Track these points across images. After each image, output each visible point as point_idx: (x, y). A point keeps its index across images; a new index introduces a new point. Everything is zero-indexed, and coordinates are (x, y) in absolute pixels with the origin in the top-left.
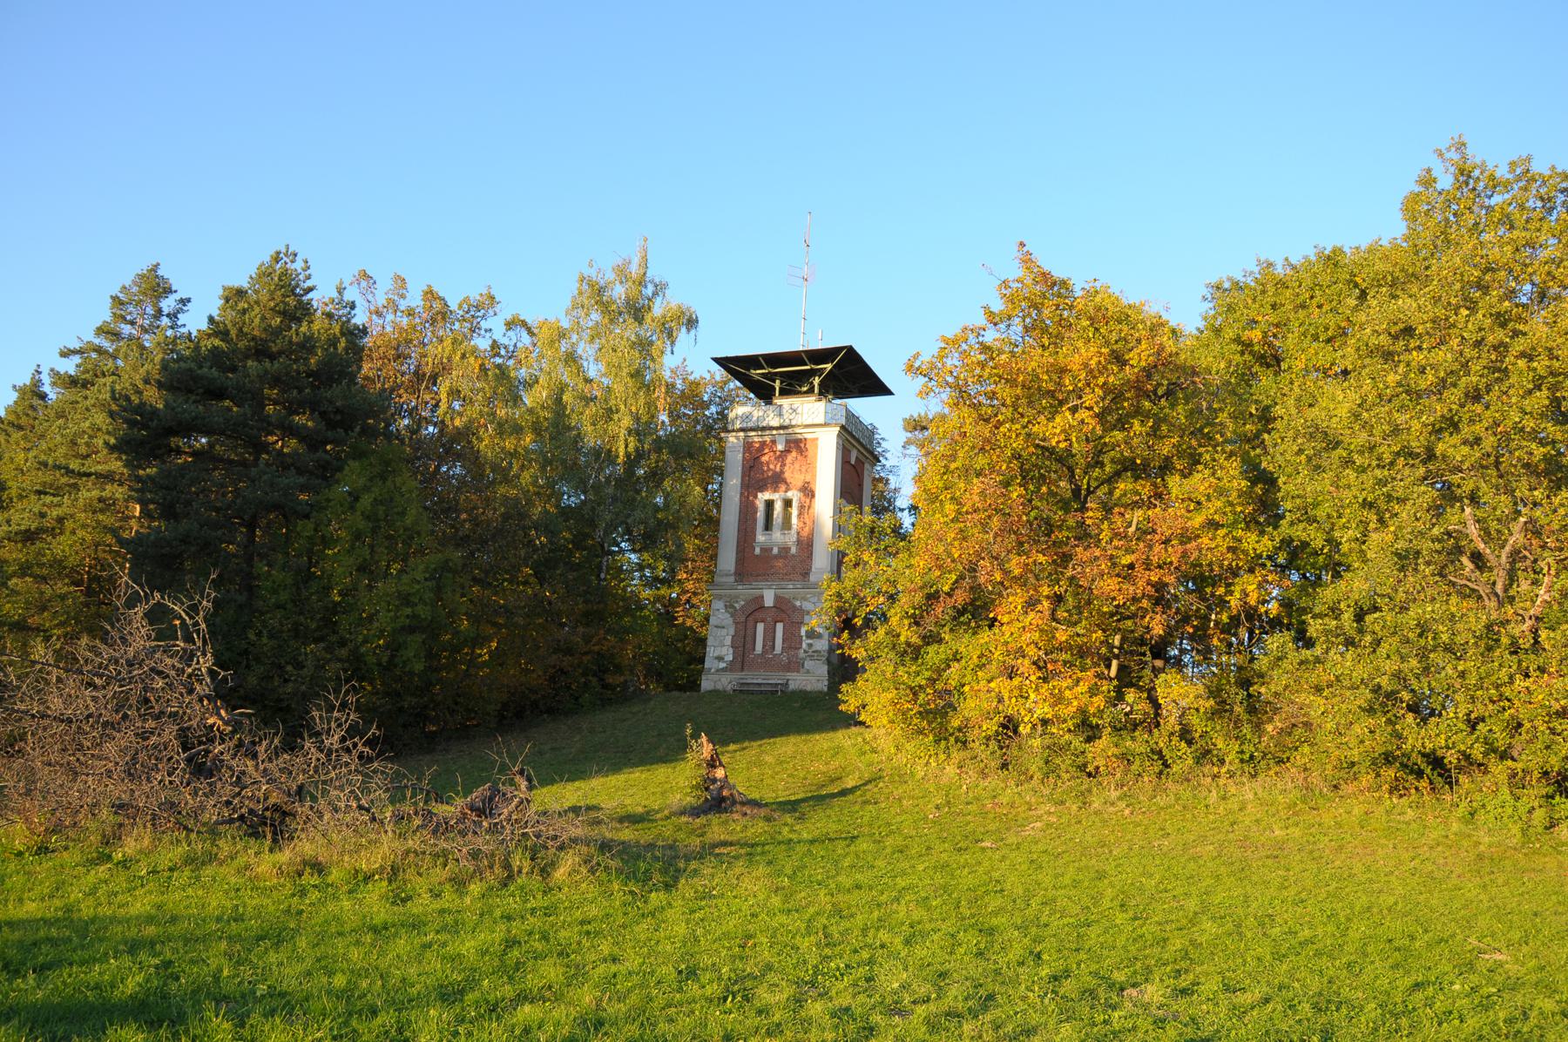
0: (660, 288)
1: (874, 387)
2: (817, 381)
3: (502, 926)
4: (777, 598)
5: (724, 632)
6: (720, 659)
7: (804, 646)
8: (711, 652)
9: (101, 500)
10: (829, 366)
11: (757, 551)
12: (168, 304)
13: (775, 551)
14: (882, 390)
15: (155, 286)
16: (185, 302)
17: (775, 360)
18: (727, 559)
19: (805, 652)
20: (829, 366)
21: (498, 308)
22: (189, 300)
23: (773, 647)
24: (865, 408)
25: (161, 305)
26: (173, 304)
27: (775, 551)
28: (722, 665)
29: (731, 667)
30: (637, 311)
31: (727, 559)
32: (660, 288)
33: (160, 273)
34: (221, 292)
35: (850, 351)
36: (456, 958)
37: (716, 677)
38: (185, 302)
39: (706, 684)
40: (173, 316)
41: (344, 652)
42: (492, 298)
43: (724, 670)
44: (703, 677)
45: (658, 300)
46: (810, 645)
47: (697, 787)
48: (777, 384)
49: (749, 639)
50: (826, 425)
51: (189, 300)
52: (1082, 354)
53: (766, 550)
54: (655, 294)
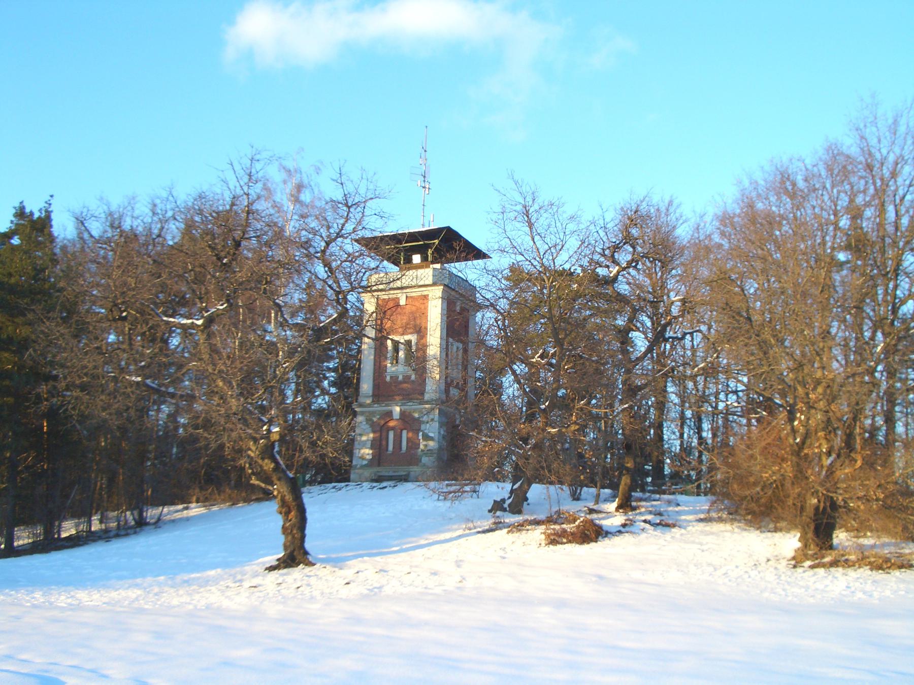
1: (473, 253)
3: (907, 215)
4: (402, 413)
7: (422, 447)
10: (436, 241)
11: (388, 379)
13: (401, 378)
14: (479, 254)
17: (413, 236)
18: (366, 386)
19: (422, 451)
23: (401, 448)
24: (469, 271)
27: (401, 378)
28: (365, 462)
31: (366, 386)
35: (449, 230)
36: (632, 401)
37: (361, 471)
43: (366, 466)
44: (352, 472)
46: (426, 446)
49: (384, 443)
53: (394, 378)
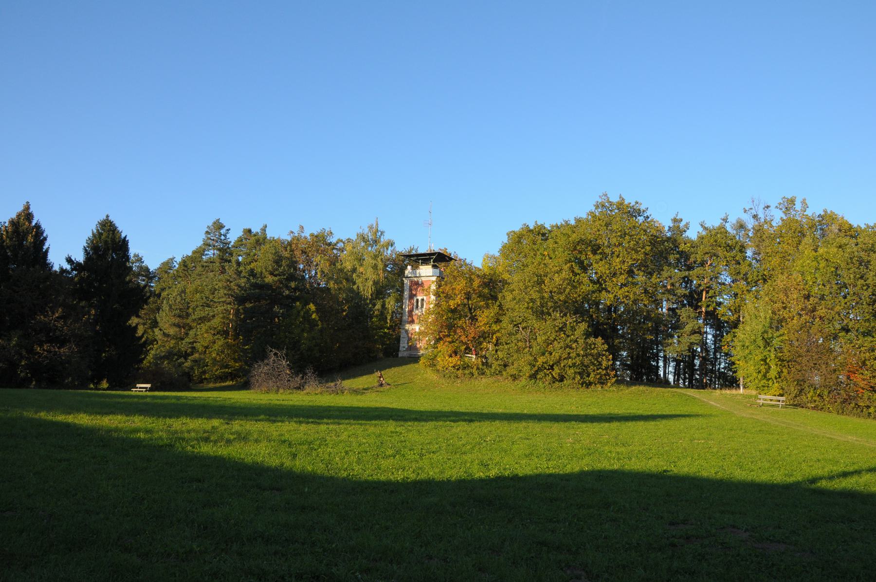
0: (382, 233)
2: (432, 260)
5: (405, 339)
6: (404, 347)
8: (401, 345)
9: (225, 310)
12: (223, 231)
15: (218, 226)
16: (228, 230)
20: (434, 257)
21: (334, 236)
22: (230, 229)
25: (221, 232)
26: (225, 231)
29: (407, 350)
30: (376, 242)
32: (382, 233)
33: (220, 221)
34: (242, 230)
38: (228, 230)
39: (400, 355)
40: (225, 236)
41: (299, 352)
42: (331, 233)
45: (382, 237)
47: (351, 395)
48: (420, 261)
50: (433, 276)
51: (230, 229)
52: (476, 283)
54: (381, 234)
